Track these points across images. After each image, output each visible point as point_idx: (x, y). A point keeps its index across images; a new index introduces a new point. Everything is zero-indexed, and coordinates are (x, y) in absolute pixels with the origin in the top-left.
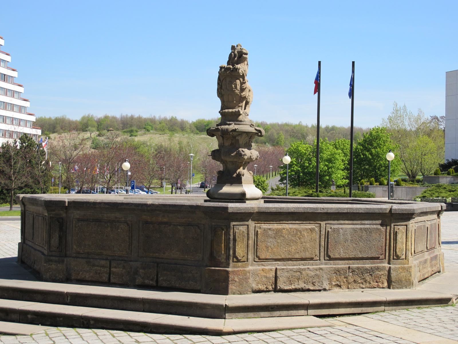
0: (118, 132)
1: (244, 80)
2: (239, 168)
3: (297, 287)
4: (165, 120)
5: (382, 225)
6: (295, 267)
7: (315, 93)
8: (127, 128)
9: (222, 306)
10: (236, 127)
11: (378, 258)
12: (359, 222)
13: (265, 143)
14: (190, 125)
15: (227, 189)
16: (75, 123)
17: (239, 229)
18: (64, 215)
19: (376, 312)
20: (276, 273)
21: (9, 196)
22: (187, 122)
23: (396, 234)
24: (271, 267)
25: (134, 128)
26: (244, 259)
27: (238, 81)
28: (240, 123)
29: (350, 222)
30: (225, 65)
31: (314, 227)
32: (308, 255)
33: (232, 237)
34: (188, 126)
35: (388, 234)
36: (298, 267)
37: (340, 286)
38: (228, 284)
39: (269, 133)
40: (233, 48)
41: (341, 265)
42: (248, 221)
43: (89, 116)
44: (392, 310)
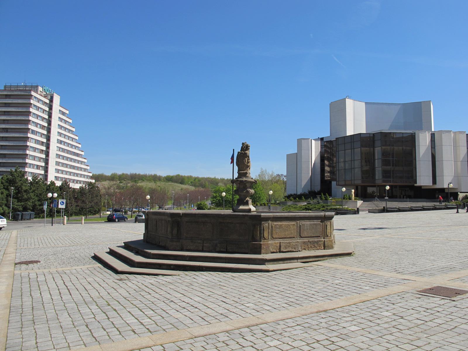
0: (129, 181)
1: (249, 158)
2: (247, 198)
3: (289, 250)
4: (151, 175)
5: (321, 222)
6: (287, 241)
7: (231, 163)
8: (133, 179)
9: (264, 259)
10: (246, 179)
11: (319, 237)
12: (312, 221)
13: (199, 187)
14: (163, 178)
15: (241, 207)
16: (108, 176)
17: (265, 224)
18: (180, 220)
19: (324, 260)
20: (280, 244)
21: (83, 212)
22: (162, 176)
23: (326, 226)
24: (277, 241)
25: (137, 179)
26: (267, 238)
27: (246, 159)
28: (247, 177)
29: (309, 221)
30: (240, 151)
31: (295, 223)
32: (292, 236)
33: (262, 228)
34: (162, 179)
35: (323, 226)
36: (289, 241)
37: (305, 249)
38: (261, 249)
39: (201, 182)
40: (243, 144)
41: (305, 240)
42: (269, 221)
43: (115, 173)
44: (330, 259)
